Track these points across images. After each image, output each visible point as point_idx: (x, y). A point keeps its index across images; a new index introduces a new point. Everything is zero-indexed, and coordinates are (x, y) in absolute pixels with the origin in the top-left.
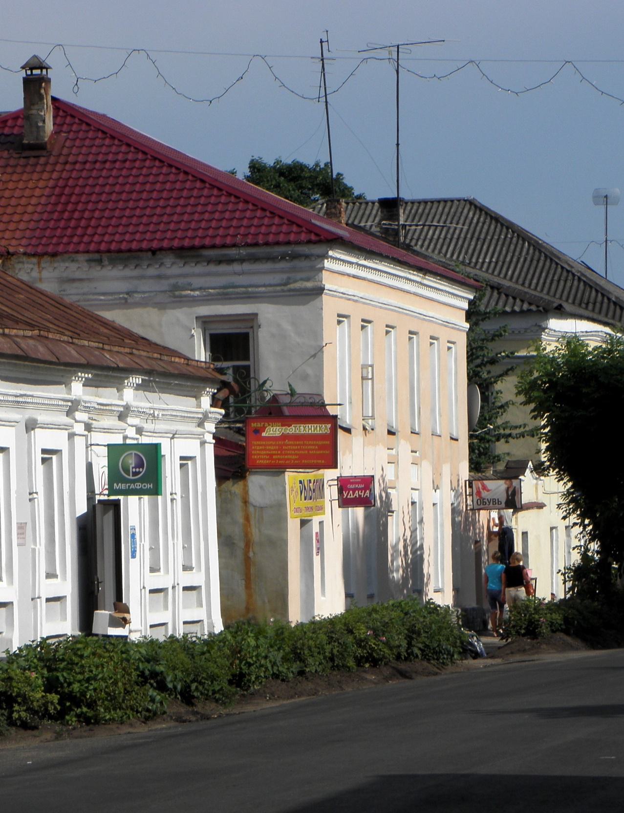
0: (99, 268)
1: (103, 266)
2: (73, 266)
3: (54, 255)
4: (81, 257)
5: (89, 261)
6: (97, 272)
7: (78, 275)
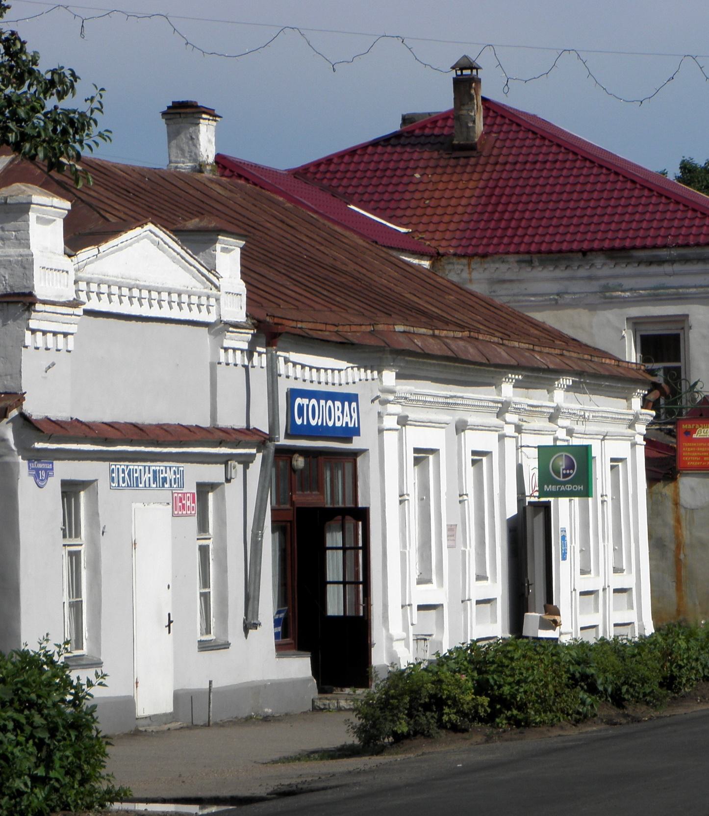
0: (529, 269)
1: (533, 267)
2: (503, 267)
3: (484, 256)
4: (512, 258)
5: (519, 262)
6: (527, 273)
7: (508, 276)
